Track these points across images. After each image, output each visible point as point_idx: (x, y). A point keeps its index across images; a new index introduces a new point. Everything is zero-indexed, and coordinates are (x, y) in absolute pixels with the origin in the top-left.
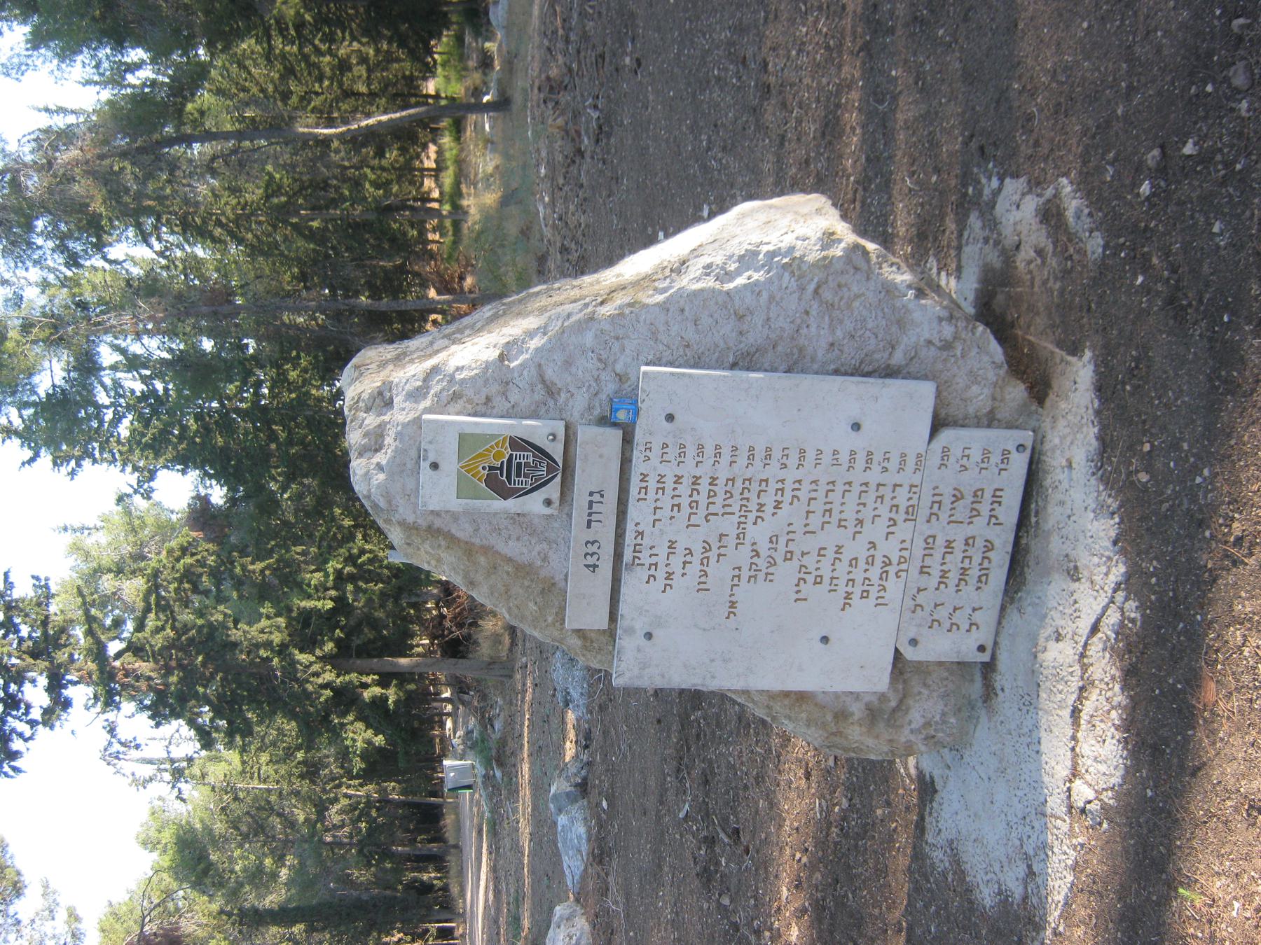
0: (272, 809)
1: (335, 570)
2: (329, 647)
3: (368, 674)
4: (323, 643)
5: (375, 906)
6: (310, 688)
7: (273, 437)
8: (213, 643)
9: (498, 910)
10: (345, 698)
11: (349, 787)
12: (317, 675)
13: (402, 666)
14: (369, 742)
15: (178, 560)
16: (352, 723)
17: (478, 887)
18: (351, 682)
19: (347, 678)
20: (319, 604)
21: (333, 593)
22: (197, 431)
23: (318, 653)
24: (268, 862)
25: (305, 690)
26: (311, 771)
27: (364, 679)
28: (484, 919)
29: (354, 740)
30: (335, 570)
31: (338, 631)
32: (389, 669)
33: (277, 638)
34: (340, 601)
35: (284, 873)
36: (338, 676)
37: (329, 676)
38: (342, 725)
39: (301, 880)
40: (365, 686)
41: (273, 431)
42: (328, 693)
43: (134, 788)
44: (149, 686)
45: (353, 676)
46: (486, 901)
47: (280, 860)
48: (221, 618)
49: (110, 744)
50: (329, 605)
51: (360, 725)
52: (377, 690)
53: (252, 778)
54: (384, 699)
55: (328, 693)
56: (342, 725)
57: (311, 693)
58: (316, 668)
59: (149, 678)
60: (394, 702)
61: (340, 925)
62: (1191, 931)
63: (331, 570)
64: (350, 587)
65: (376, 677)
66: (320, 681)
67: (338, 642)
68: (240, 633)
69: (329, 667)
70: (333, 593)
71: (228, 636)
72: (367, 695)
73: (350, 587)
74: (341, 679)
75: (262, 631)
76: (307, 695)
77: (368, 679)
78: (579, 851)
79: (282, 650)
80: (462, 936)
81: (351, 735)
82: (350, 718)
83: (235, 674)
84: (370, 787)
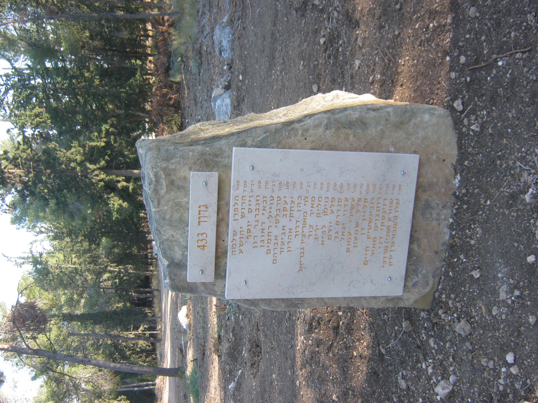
0: (77, 273)
1: (106, 129)
2: (103, 163)
3: (120, 176)
4: (100, 161)
5: (122, 313)
6: (94, 181)
7: (78, 102)
8: (49, 160)
9: (177, 300)
10: (110, 187)
11: (111, 267)
12: (97, 175)
13: (136, 174)
14: (121, 206)
15: (34, 120)
16: (113, 197)
17: (168, 300)
18: (112, 179)
19: (111, 177)
20: (98, 144)
21: (105, 140)
22: (43, 97)
23: (98, 166)
24: (75, 296)
25: (91, 182)
26: (94, 260)
27: (118, 179)
28: (170, 311)
29: (114, 205)
30: (106, 129)
31: (107, 157)
32: (129, 175)
33: (79, 158)
34: (108, 143)
35: (83, 301)
36: (107, 177)
37: (103, 176)
38: (108, 198)
39: (90, 304)
40: (119, 182)
41: (78, 99)
42: (102, 183)
43: (16, 266)
44: (20, 180)
45: (114, 176)
46: (172, 296)
47: (80, 296)
48: (53, 146)
49: (2, 205)
50: (103, 144)
51: (116, 198)
52: (124, 184)
53: (68, 263)
54: (127, 188)
55: (102, 183)
56: (108, 198)
57: (94, 183)
58: (96, 172)
59: (20, 176)
60: (132, 189)
61: (107, 321)
62: (529, 109)
63: (103, 129)
64: (112, 137)
65: (124, 178)
66: (98, 178)
67: (107, 162)
68: (62, 153)
69: (102, 173)
70: (105, 140)
71: (56, 154)
72: (119, 185)
73: (112, 137)
74: (108, 177)
75: (72, 154)
76: (93, 184)
77: (120, 179)
78: (226, 113)
79: (81, 164)
80: (161, 329)
81: (112, 202)
82: (112, 195)
83: (59, 174)
84: (120, 267)
